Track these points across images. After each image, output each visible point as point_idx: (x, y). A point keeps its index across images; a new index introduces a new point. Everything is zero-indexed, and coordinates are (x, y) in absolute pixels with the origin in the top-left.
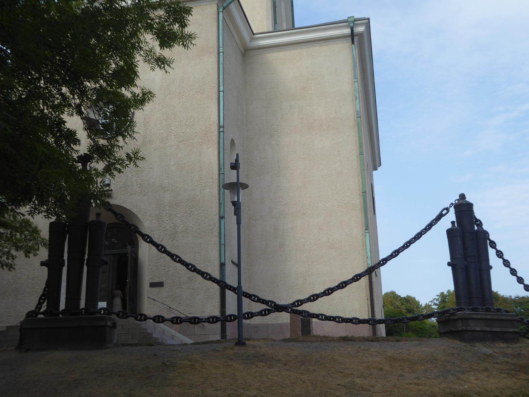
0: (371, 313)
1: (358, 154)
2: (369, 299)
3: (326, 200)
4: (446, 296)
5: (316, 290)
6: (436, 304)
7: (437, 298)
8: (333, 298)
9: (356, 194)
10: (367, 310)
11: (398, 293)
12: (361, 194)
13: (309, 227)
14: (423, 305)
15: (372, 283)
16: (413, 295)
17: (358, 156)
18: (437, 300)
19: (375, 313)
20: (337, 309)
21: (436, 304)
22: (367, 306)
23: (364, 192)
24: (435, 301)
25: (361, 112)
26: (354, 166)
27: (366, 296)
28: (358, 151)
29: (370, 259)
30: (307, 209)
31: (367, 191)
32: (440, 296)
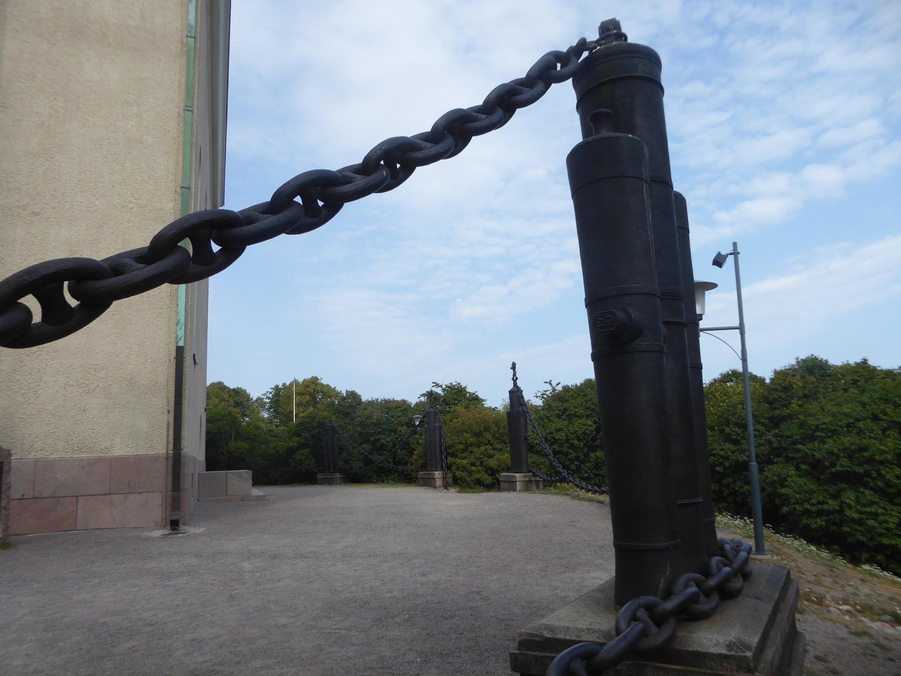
0: (172, 441)
1: (182, 111)
2: (172, 413)
3: (96, 191)
4: (281, 389)
5: (45, 387)
6: (269, 398)
7: (271, 391)
8: (87, 407)
9: (167, 189)
10: (166, 435)
11: (227, 384)
12: (179, 190)
13: (44, 245)
14: (254, 399)
15: (182, 378)
16: (244, 387)
17: (182, 113)
18: (270, 393)
19: (182, 442)
20: (93, 432)
21: (269, 398)
22: (165, 425)
23: (183, 188)
24: (268, 394)
25: (199, 31)
26: (170, 132)
27: (166, 404)
28: (182, 105)
29: (183, 328)
30: (46, 204)
31: (193, 186)
32: (274, 389)
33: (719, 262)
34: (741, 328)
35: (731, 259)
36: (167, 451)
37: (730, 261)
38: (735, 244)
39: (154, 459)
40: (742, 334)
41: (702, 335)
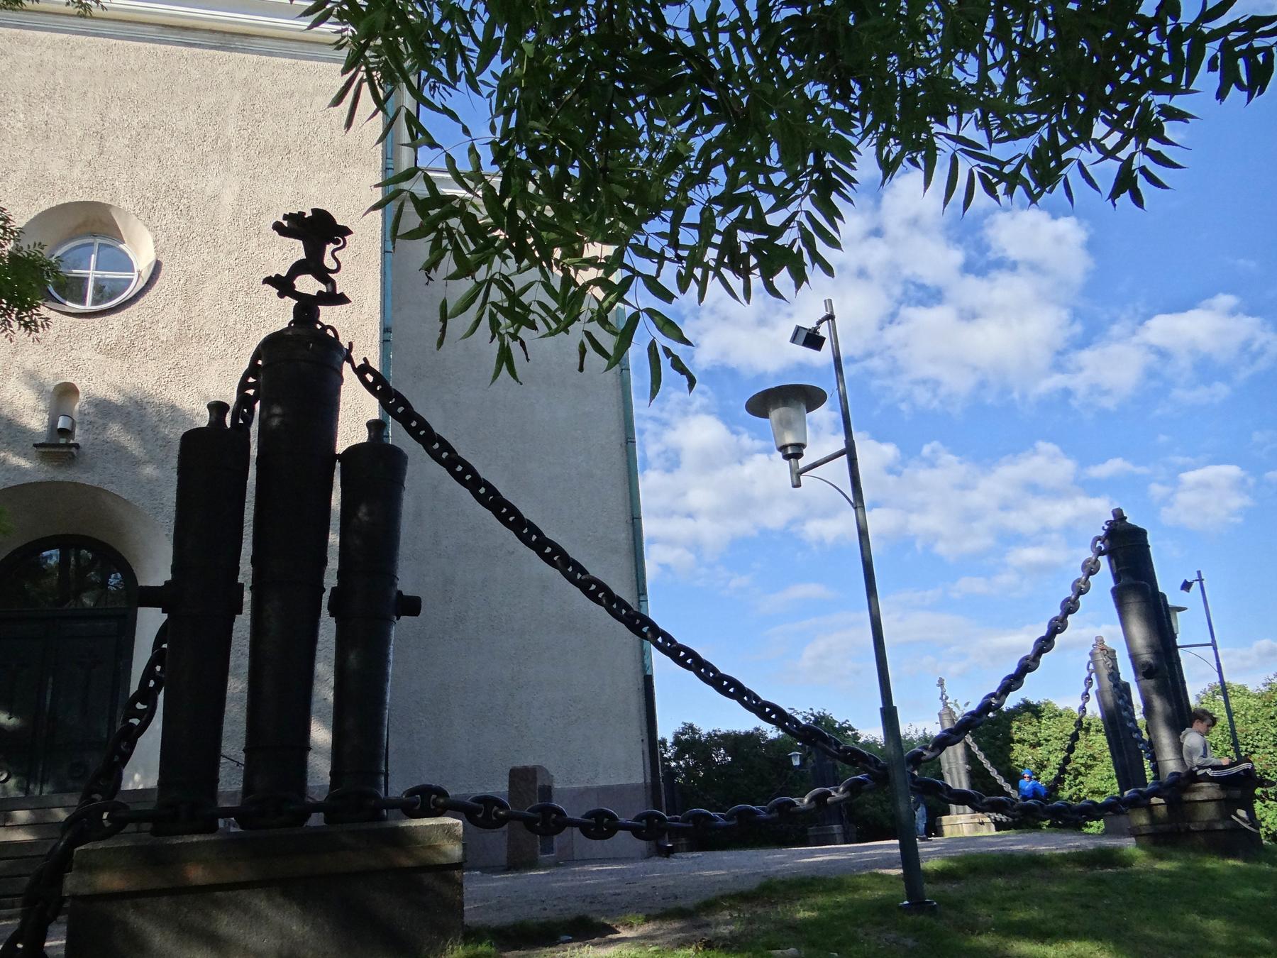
2: (646, 741)
33: (1186, 586)
34: (1213, 644)
35: (1196, 585)
36: (645, 780)
37: (1196, 585)
38: (1199, 573)
39: (635, 788)
40: (1215, 649)
41: (1180, 651)
